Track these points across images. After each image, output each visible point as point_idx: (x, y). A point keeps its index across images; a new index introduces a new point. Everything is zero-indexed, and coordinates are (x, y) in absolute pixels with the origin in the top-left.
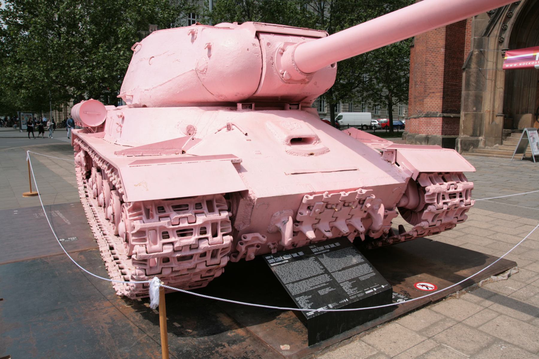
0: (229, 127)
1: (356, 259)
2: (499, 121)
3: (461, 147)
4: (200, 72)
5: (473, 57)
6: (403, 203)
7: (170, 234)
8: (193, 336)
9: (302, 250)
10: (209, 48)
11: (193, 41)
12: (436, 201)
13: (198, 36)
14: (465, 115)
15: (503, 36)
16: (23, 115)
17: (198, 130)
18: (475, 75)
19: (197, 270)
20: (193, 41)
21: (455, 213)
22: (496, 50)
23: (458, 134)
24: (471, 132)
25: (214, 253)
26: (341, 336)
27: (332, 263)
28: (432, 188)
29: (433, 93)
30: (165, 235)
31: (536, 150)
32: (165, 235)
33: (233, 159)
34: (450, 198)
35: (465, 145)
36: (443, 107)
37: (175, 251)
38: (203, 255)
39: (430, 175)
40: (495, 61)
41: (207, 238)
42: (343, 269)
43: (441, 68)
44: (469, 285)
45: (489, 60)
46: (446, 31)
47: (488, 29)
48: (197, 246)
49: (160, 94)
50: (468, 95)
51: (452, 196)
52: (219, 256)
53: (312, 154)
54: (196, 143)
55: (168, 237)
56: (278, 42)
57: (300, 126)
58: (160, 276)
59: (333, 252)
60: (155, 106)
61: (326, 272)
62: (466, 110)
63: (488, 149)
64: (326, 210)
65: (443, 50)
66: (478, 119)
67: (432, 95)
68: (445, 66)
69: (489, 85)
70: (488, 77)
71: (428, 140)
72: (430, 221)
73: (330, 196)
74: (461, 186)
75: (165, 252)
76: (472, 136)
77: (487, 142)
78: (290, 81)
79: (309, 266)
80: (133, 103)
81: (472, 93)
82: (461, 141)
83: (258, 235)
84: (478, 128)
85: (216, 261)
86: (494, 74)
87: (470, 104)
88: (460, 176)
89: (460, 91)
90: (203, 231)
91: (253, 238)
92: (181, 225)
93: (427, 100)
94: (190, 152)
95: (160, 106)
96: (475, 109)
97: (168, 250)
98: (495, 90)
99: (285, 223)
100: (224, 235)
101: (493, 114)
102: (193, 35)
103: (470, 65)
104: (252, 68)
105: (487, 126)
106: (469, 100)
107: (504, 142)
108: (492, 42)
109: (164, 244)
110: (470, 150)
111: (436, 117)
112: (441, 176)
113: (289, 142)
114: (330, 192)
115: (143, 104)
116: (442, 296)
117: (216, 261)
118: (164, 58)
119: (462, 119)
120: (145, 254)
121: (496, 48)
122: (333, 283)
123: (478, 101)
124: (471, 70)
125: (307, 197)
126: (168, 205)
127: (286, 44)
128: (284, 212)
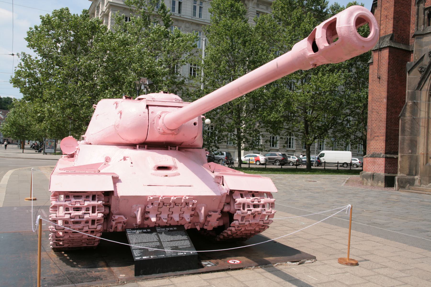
0: (125, 159)
1: (185, 237)
3: (398, 184)
4: (116, 126)
7: (70, 209)
8: (80, 268)
9: (147, 228)
11: (116, 108)
12: (242, 208)
16: (47, 141)
17: (112, 159)
18: (409, 122)
21: (260, 217)
22: (427, 102)
23: (397, 173)
24: (407, 171)
25: (93, 222)
26: (157, 275)
27: (164, 237)
28: (239, 200)
29: (378, 136)
33: (114, 175)
34: (254, 207)
35: (402, 182)
36: (386, 149)
37: (71, 218)
38: (87, 222)
40: (427, 111)
41: (89, 213)
42: (171, 241)
44: (264, 264)
45: (422, 110)
46: (388, 85)
47: (420, 84)
48: (83, 217)
50: (403, 139)
51: (255, 206)
52: (96, 224)
53: (166, 176)
54: (107, 166)
55: (69, 210)
58: (63, 231)
59: (170, 233)
60: (95, 144)
61: (159, 241)
62: (402, 152)
63: (423, 187)
65: (385, 100)
67: (377, 138)
68: (387, 114)
70: (421, 124)
71: (373, 177)
72: (240, 220)
73: (164, 198)
75: (66, 217)
76: (408, 175)
77: (422, 181)
78: (164, 133)
81: (407, 137)
82: (398, 179)
83: (123, 217)
84: (414, 168)
85: (94, 226)
86: (426, 122)
87: (405, 147)
88: (269, 195)
91: (119, 218)
92: (255, 203)
94: (101, 172)
96: (410, 151)
97: (67, 216)
99: (138, 211)
100: (98, 213)
101: (427, 156)
103: (405, 114)
104: (148, 125)
106: (405, 144)
109: (66, 214)
111: (380, 157)
112: (251, 193)
113: (156, 168)
114: (164, 196)
115: (90, 142)
116: (241, 267)
118: (111, 114)
119: (399, 159)
120: (55, 217)
121: (427, 100)
123: (413, 144)
125: (150, 198)
126: (72, 195)
128: (139, 205)
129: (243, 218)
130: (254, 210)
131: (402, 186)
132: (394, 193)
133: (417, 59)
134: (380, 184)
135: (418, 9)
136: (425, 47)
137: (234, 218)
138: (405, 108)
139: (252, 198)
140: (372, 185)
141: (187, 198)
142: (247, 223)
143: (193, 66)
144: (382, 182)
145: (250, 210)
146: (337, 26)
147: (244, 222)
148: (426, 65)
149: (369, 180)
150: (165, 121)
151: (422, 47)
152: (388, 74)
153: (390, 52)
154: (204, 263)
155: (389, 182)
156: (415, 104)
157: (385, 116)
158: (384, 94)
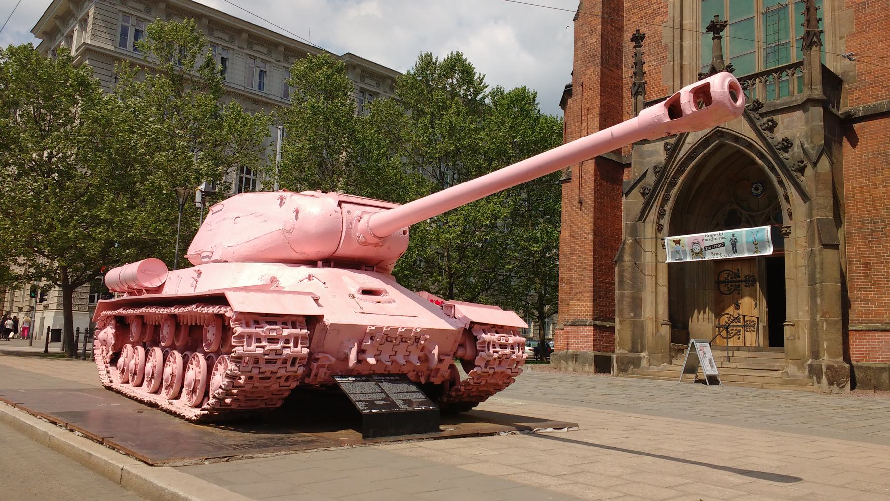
2: (666, 331)
5: (626, 247)
6: (460, 352)
10: (297, 212)
11: (281, 205)
13: (287, 201)
14: (621, 322)
15: (662, 222)
18: (630, 270)
19: (272, 389)
20: (281, 205)
24: (629, 345)
26: (392, 438)
30: (259, 340)
31: (709, 369)
32: (259, 340)
38: (285, 361)
39: (483, 327)
43: (589, 260)
46: (595, 213)
47: (643, 212)
49: (245, 250)
50: (622, 296)
51: (503, 346)
56: (357, 211)
57: (373, 282)
60: (238, 261)
61: (383, 391)
62: (621, 315)
63: (654, 368)
64: (387, 343)
65: (591, 237)
66: (638, 328)
67: (579, 296)
69: (649, 282)
72: (483, 367)
74: (512, 339)
76: (631, 351)
78: (365, 244)
79: (371, 386)
80: (213, 259)
81: (627, 293)
82: (617, 358)
85: (294, 369)
89: (612, 292)
90: (287, 341)
93: (574, 303)
95: (243, 261)
96: (632, 314)
97: (260, 351)
98: (656, 290)
101: (656, 321)
102: (282, 200)
103: (623, 257)
104: (332, 232)
105: (650, 338)
107: (674, 360)
108: (648, 229)
110: (630, 371)
111: (585, 326)
117: (294, 369)
119: (617, 327)
122: (387, 398)
123: (636, 304)
124: (624, 264)
127: (364, 212)
129: (487, 363)
130: (502, 351)
131: (623, 370)
132: (612, 381)
133: (638, 175)
134: (587, 368)
135: (636, 103)
136: (648, 159)
137: (476, 364)
138: (623, 248)
139: (497, 335)
140: (574, 371)
141: (418, 330)
142: (492, 371)
143: (245, 175)
144: (590, 365)
145: (497, 352)
146: (711, 90)
147: (488, 370)
148: (650, 185)
149: (570, 363)
150: (371, 224)
151: (643, 159)
152: (595, 197)
153: (596, 163)
154: (441, 427)
155: (602, 365)
156: (637, 242)
157: (590, 260)
158: (590, 227)
